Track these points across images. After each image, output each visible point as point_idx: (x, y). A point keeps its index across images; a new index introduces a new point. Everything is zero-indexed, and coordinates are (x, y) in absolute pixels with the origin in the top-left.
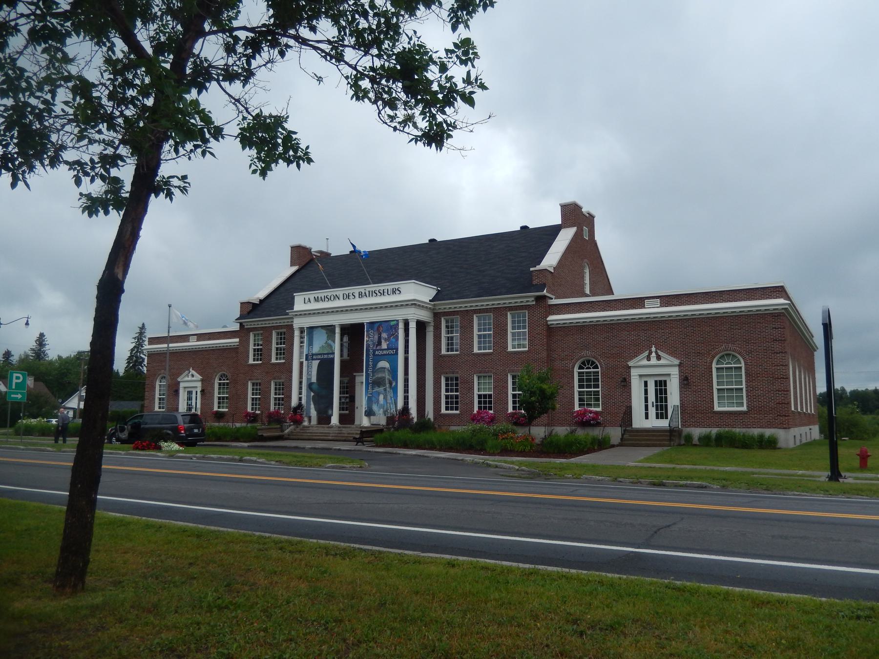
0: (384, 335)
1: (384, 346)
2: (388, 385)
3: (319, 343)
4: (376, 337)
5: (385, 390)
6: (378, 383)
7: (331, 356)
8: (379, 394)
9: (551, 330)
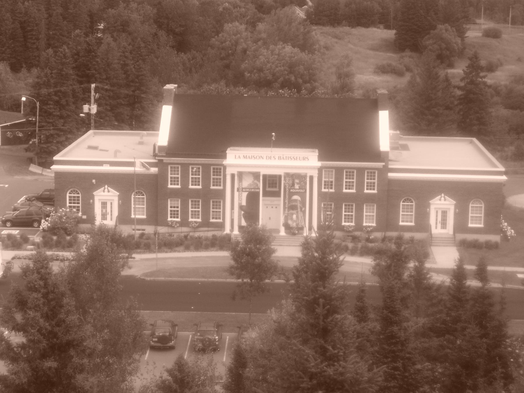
0: (297, 181)
1: (297, 187)
2: (299, 210)
3: (247, 182)
4: (291, 182)
5: (297, 212)
6: (293, 208)
8: (292, 214)
9: (392, 182)
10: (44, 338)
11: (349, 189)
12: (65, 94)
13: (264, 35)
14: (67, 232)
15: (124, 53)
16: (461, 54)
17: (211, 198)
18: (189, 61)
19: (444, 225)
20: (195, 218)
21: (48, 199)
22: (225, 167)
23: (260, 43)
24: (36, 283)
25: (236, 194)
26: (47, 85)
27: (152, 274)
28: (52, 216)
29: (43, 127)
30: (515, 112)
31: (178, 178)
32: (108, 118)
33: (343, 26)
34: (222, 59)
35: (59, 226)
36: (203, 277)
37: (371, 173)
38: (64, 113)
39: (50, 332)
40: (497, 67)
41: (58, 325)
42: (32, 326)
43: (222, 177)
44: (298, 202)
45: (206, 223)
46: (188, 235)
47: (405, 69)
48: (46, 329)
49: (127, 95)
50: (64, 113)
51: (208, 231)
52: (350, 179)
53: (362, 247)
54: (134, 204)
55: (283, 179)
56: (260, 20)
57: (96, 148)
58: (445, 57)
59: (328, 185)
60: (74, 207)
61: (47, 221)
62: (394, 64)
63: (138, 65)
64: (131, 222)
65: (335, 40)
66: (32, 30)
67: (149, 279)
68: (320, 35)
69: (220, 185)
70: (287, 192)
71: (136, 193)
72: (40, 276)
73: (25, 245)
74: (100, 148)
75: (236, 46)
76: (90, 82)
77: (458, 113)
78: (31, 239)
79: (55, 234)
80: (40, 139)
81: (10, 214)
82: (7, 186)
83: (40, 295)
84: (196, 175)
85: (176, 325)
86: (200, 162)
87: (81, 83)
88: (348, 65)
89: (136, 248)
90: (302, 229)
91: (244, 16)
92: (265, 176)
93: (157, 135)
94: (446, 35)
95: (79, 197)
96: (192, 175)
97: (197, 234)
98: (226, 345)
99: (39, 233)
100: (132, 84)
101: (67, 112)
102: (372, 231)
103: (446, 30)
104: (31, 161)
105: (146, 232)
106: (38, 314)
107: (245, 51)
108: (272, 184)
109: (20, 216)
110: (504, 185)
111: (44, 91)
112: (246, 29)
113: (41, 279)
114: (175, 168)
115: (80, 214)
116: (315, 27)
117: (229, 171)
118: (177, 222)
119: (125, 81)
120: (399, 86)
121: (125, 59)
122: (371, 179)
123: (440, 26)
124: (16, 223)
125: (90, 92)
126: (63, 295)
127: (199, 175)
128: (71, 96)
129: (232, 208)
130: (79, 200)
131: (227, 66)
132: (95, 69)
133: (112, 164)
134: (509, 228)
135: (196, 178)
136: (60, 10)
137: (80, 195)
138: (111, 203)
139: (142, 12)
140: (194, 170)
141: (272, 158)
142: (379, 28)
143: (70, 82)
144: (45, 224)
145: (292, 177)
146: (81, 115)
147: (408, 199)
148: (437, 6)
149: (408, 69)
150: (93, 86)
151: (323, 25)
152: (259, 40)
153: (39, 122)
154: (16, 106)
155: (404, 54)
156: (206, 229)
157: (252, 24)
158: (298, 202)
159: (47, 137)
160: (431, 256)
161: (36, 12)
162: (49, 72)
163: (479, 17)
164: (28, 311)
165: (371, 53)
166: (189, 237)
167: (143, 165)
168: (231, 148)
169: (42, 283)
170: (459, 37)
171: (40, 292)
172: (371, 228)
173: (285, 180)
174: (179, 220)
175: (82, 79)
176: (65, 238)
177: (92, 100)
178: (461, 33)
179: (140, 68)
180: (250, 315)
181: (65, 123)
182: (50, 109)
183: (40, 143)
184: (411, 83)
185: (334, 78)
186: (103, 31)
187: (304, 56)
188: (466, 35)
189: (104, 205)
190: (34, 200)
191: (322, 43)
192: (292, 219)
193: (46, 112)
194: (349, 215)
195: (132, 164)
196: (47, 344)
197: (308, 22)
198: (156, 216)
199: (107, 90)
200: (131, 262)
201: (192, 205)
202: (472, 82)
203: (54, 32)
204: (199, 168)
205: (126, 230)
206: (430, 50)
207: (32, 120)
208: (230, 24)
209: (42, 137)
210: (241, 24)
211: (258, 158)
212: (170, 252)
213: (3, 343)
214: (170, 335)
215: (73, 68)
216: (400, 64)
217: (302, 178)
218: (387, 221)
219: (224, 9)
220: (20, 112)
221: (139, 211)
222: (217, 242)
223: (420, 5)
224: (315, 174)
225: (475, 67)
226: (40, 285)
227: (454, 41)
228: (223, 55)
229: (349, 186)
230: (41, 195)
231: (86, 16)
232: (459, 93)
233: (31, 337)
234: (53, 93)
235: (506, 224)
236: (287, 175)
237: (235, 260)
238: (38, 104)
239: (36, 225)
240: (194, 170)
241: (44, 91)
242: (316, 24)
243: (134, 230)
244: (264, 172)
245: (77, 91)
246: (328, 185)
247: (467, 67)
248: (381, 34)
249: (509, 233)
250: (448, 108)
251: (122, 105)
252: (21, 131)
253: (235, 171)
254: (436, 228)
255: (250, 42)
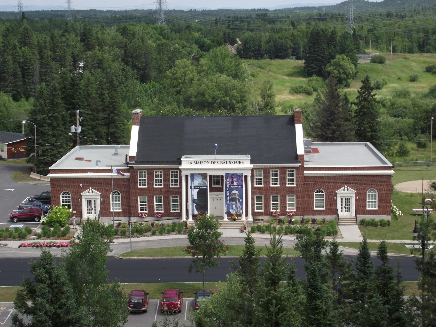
0: (235, 179)
1: (235, 184)
2: (238, 201)
3: (198, 182)
4: (231, 181)
5: (236, 203)
6: (233, 200)
7: (206, 188)
8: (233, 205)
9: (307, 177)
10: (49, 318)
11: (275, 184)
12: (56, 118)
13: (205, 68)
14: (61, 224)
15: (100, 85)
16: (355, 76)
17: (171, 194)
18: (150, 89)
19: (348, 209)
20: (159, 210)
21: (46, 199)
22: (180, 171)
23: (202, 74)
24: (42, 276)
25: (190, 190)
26: (42, 112)
27: (127, 254)
28: (50, 212)
29: (40, 144)
30: (398, 119)
31: (145, 180)
32: (89, 136)
33: (265, 58)
34: (175, 86)
35: (55, 220)
36: (167, 255)
37: (291, 171)
38: (56, 132)
39: (54, 314)
40: (383, 85)
41: (60, 308)
42: (40, 310)
43: (178, 178)
44: (237, 195)
45: (167, 214)
46: (154, 223)
47: (313, 89)
48: (51, 312)
49: (104, 117)
50: (56, 132)
51: (169, 219)
52: (275, 176)
53: (286, 228)
54: (112, 201)
55: (224, 178)
56: (202, 56)
57: (81, 159)
58: (342, 81)
59: (259, 181)
60: (66, 205)
61: (45, 216)
62: (304, 86)
63: (112, 95)
64: (110, 214)
65: (259, 69)
66: (28, 69)
67: (125, 258)
68: (246, 65)
69: (177, 185)
70: (228, 188)
71: (114, 192)
72: (45, 271)
73: (28, 236)
74: (84, 159)
75: (185, 76)
76: (75, 109)
77: (355, 123)
78: (34, 231)
79: (52, 226)
80: (38, 153)
81: (17, 212)
82: (13, 190)
83: (46, 285)
84: (158, 177)
85: (148, 294)
86: (161, 168)
87: (68, 110)
88: (270, 88)
89: (115, 235)
90: (240, 215)
91: (189, 54)
92: (211, 176)
93: (129, 147)
94: (342, 63)
95: (69, 197)
96: (156, 177)
97: (161, 222)
98: (186, 308)
99: (39, 226)
100: (107, 109)
101: (58, 132)
102: (293, 215)
103: (343, 59)
104: (31, 170)
105: (122, 222)
106: (45, 300)
107: (192, 80)
108: (216, 182)
109: (24, 213)
110: (392, 177)
111: (40, 117)
112: (192, 63)
113: (46, 273)
114: (142, 172)
115: (71, 210)
116: (243, 60)
117: (184, 174)
118: (145, 213)
119: (102, 107)
120: (308, 103)
121: (102, 90)
122: (291, 176)
123: (338, 56)
124: (21, 218)
125: (76, 116)
126: (64, 284)
127: (161, 177)
128: (61, 120)
129: (187, 202)
130: (70, 200)
131: (178, 92)
132: (79, 99)
133: (94, 171)
134: (397, 209)
135: (159, 180)
136: (50, 53)
137: (70, 196)
138: (95, 201)
139: (112, 53)
140: (157, 174)
141: (216, 163)
142: (292, 59)
143: (60, 109)
144: (44, 219)
145: (231, 177)
146: (69, 134)
147: (319, 190)
148: (335, 41)
149: (315, 90)
150: (78, 111)
151: (250, 58)
152: (202, 71)
153: (37, 140)
154: (18, 127)
155: (311, 78)
156: (168, 218)
157: (197, 60)
158: (237, 195)
159: (44, 152)
160: (339, 233)
161: (31, 54)
162: (43, 101)
163: (367, 47)
164: (36, 298)
165: (286, 78)
166: (155, 225)
167: (118, 171)
168: (185, 156)
169: (47, 276)
170: (353, 64)
171: (46, 283)
172: (293, 213)
173: (226, 179)
174: (147, 212)
175: (69, 107)
176: (60, 229)
177: (78, 123)
178: (355, 62)
179: (113, 97)
180: (204, 283)
181: (56, 140)
182: (45, 130)
183: (38, 156)
184: (317, 100)
185: (259, 99)
186: (84, 68)
187: (236, 82)
188: (358, 62)
189: (89, 202)
190: (35, 200)
191: (249, 72)
192: (232, 208)
193: (41, 132)
194: (275, 204)
195: (110, 171)
196: (52, 323)
197: (238, 57)
198: (129, 210)
199: (88, 114)
200: (112, 246)
201: (156, 200)
202: (365, 99)
203: (45, 70)
204: (161, 172)
205: (106, 222)
206: (333, 76)
207: (31, 139)
208: (179, 60)
209: (40, 151)
210: (188, 60)
211: (205, 163)
212: (141, 237)
213: (17, 323)
214: (143, 302)
215: (62, 98)
216: (309, 86)
217: (239, 177)
218: (305, 208)
219: (174, 49)
220: (21, 132)
221: (116, 207)
222: (177, 228)
223: (322, 41)
224: (249, 174)
225: (367, 87)
226: (45, 277)
227: (349, 67)
228: (175, 83)
229: (275, 182)
230: (40, 196)
231: (70, 57)
232: (355, 107)
233: (39, 319)
234: (47, 118)
235: (395, 207)
236: (227, 175)
237: (191, 242)
238: (35, 126)
239: (37, 219)
240: (157, 174)
241: (40, 117)
242: (245, 58)
243: (112, 221)
244: (210, 173)
245: (65, 115)
246: (259, 181)
247: (360, 88)
248: (293, 63)
249: (397, 214)
250: (347, 120)
251: (100, 125)
252: (23, 148)
253: (188, 173)
254: (342, 211)
255: (195, 73)
